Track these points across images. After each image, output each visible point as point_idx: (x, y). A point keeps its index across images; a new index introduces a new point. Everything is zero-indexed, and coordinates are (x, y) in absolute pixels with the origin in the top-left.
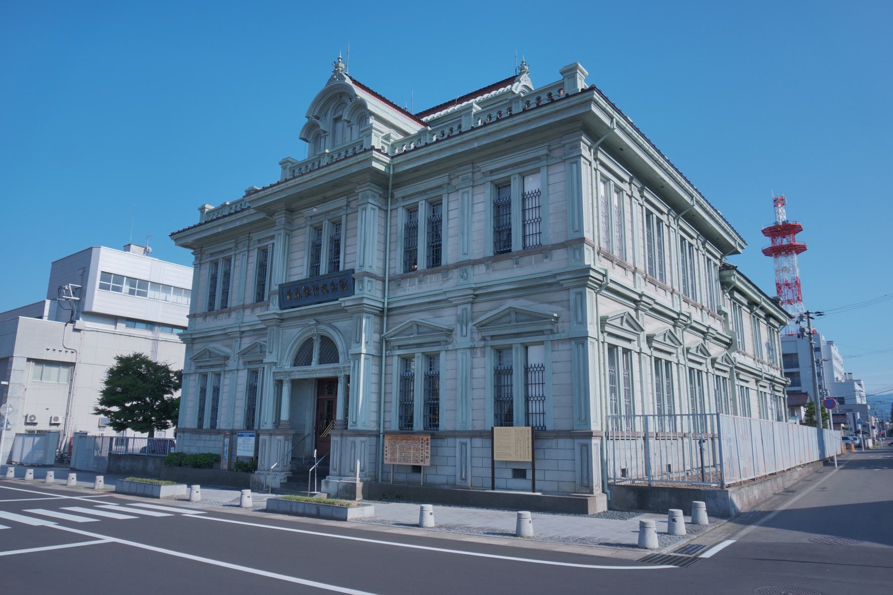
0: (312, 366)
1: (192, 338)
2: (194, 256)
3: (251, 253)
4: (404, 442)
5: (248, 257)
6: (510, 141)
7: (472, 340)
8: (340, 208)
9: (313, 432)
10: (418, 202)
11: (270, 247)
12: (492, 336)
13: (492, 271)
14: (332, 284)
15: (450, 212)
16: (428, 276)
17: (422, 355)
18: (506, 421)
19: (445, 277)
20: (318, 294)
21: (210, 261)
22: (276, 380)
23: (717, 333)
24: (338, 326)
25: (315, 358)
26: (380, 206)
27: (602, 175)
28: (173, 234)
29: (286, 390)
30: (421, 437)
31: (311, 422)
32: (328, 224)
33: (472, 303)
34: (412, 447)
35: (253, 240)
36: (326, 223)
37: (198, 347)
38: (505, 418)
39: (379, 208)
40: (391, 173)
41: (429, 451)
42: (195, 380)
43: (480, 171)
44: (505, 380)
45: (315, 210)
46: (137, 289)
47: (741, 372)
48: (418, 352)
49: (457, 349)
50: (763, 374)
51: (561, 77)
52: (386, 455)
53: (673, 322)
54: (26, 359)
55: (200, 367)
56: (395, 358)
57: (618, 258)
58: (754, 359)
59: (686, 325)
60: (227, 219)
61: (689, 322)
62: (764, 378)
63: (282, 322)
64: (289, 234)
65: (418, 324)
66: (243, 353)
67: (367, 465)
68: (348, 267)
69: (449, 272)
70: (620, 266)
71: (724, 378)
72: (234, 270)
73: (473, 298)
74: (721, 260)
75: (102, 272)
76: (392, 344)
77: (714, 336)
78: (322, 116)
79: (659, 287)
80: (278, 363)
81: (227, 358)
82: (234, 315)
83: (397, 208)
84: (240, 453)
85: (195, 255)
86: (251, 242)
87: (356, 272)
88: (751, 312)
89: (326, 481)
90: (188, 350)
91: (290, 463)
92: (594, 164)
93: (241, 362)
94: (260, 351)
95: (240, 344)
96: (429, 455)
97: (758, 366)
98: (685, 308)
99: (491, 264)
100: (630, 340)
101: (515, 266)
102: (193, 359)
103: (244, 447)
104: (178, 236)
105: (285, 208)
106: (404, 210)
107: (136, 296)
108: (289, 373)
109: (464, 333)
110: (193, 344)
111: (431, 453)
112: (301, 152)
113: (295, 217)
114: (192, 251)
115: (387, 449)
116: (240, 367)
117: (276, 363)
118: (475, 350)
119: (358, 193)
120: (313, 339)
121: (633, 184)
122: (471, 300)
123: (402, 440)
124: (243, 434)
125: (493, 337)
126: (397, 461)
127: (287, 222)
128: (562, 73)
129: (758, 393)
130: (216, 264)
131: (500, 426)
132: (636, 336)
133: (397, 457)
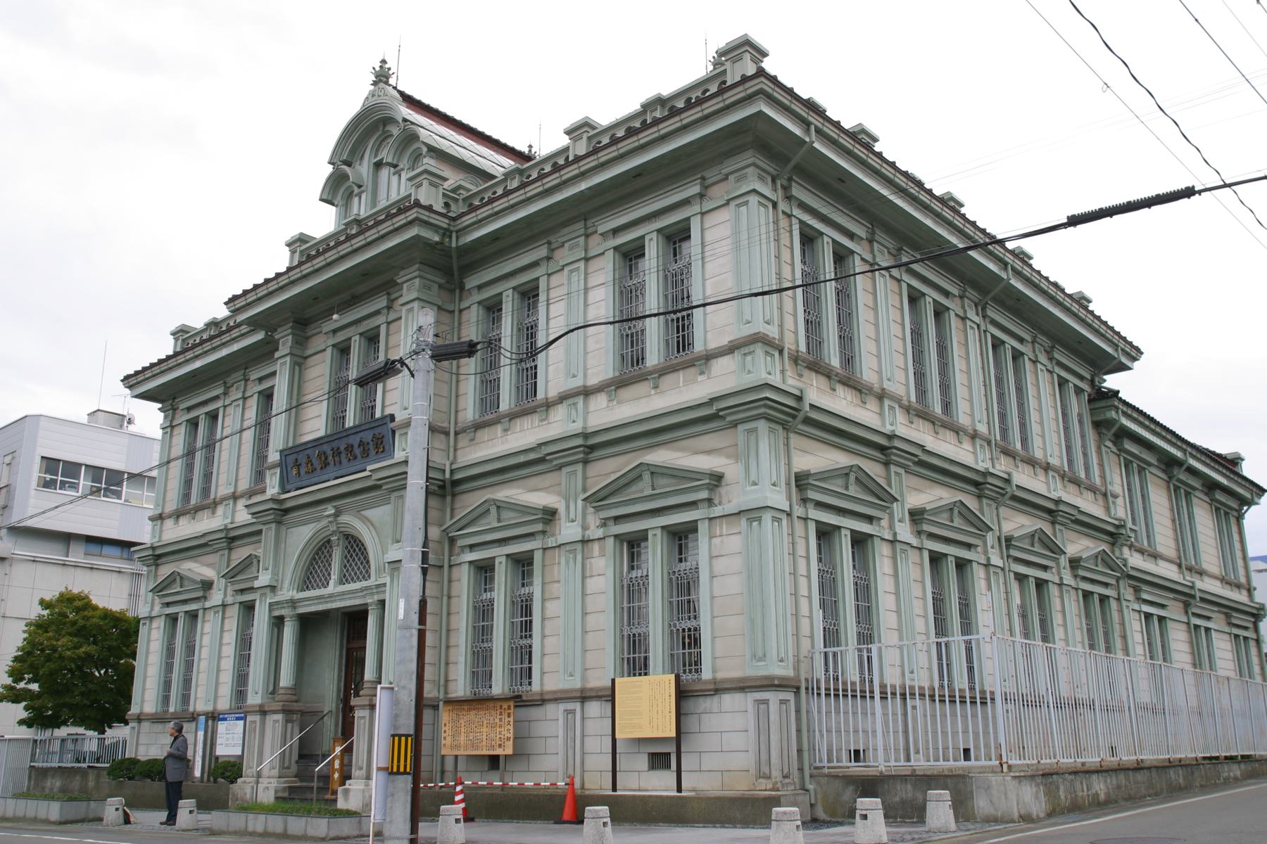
1: (156, 555)
2: (163, 414)
4: (473, 713)
6: (639, 175)
7: (585, 528)
9: (337, 708)
13: (619, 403)
14: (361, 444)
17: (507, 560)
19: (544, 420)
20: (340, 463)
21: (187, 421)
23: (1080, 512)
24: (374, 520)
25: (334, 574)
26: (440, 304)
28: (127, 378)
29: (289, 632)
31: (335, 689)
32: (360, 342)
33: (586, 462)
34: (485, 723)
36: (355, 341)
38: (637, 665)
41: (511, 728)
43: (596, 232)
46: (60, 478)
47: (1144, 587)
48: (499, 553)
50: (1197, 592)
52: (445, 738)
53: (977, 491)
55: (168, 604)
56: (465, 567)
57: (839, 371)
58: (1180, 566)
60: (207, 346)
62: (1198, 599)
63: (284, 515)
64: (300, 362)
65: (498, 504)
68: (388, 411)
69: (549, 411)
70: (849, 386)
71: (1246, 638)
73: (584, 452)
74: (1092, 382)
75: (42, 457)
76: (460, 543)
77: (1074, 518)
78: (356, 161)
79: (941, 426)
80: (279, 587)
81: (207, 585)
82: (220, 510)
84: (220, 751)
85: (164, 412)
88: (1170, 478)
91: (297, 762)
92: (782, 206)
93: (229, 592)
96: (511, 735)
97: (1188, 578)
98: (1002, 466)
99: (615, 390)
100: (1045, 568)
102: (156, 590)
104: (133, 381)
105: (292, 320)
107: (103, 499)
108: (293, 603)
109: (572, 516)
110: (157, 565)
111: (514, 734)
113: (309, 334)
115: (446, 729)
117: (274, 587)
121: (878, 242)
122: (581, 456)
124: (226, 716)
125: (617, 519)
126: (462, 750)
127: (297, 343)
128: (568, 132)
129: (1189, 627)
132: (980, 539)
133: (462, 743)
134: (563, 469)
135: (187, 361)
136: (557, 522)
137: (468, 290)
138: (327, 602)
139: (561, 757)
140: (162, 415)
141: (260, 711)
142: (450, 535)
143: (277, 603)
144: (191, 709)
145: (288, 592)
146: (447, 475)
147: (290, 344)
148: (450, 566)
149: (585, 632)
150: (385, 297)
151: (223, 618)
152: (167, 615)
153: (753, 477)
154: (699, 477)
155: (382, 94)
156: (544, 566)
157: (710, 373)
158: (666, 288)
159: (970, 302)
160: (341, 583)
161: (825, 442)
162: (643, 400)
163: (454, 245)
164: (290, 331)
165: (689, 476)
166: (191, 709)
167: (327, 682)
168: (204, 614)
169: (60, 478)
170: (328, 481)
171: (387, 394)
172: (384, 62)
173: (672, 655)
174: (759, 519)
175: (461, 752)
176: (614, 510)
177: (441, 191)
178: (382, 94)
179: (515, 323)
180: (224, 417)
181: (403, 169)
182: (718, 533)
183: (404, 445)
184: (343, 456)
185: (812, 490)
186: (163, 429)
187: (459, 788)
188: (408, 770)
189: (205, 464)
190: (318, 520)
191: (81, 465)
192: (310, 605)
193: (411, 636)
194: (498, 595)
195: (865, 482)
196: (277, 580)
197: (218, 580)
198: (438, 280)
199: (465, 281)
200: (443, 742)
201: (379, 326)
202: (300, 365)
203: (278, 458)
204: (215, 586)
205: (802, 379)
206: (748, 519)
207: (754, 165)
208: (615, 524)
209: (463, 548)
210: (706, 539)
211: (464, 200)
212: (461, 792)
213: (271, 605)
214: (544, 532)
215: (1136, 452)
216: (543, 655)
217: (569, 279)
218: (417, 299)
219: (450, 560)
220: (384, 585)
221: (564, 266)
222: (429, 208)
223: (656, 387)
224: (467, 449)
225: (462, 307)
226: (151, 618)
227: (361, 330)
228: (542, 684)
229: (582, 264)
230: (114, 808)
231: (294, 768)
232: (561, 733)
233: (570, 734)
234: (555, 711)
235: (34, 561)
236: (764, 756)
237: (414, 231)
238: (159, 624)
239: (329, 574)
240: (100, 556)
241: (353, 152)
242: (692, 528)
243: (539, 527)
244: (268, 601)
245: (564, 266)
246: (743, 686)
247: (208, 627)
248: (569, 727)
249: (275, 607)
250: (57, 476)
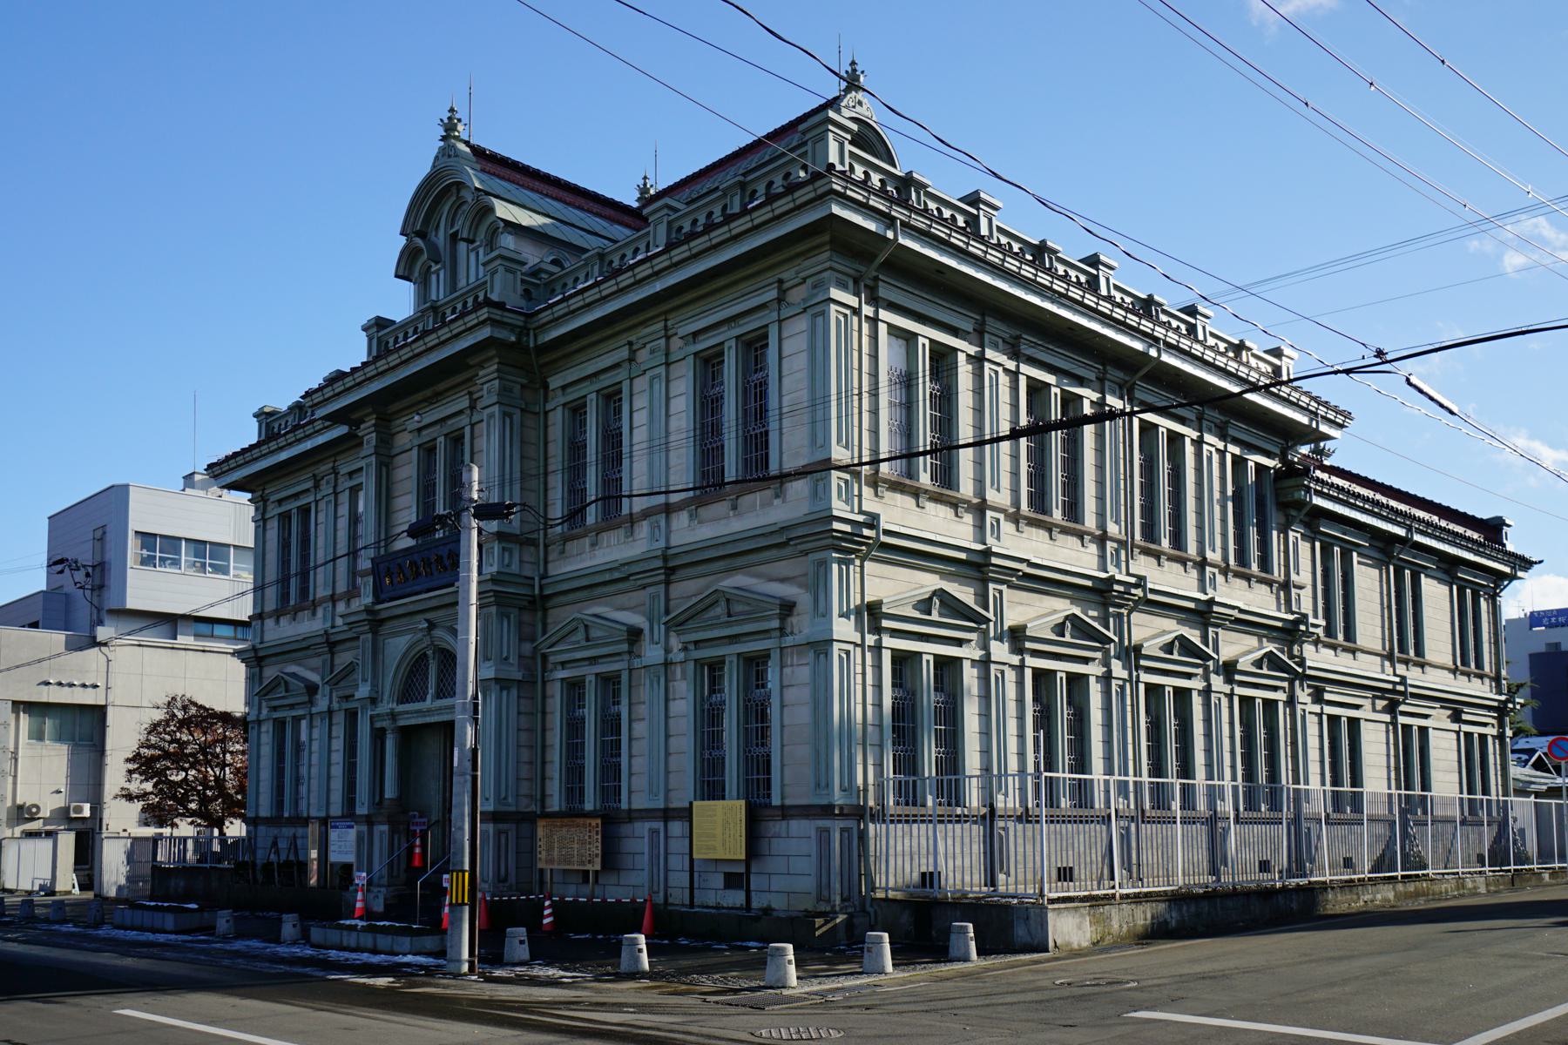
3: (676, 370)
5: (668, 381)
7: (667, 650)
8: (460, 412)
11: (591, 400)
12: (696, 643)
13: (699, 523)
16: (605, 535)
20: (432, 574)
26: (523, 406)
27: (894, 330)
28: (210, 466)
30: (588, 821)
37: (270, 673)
38: (712, 789)
40: (532, 345)
41: (599, 845)
48: (589, 672)
52: (540, 853)
54: (10, 703)
55: (275, 709)
56: (558, 685)
63: (380, 626)
72: (316, 529)
73: (665, 573)
75: (136, 532)
82: (643, 529)
84: (334, 857)
86: (268, 503)
90: (251, 679)
93: (675, 643)
94: (584, 636)
96: (599, 852)
101: (731, 513)
103: (340, 847)
104: (217, 470)
108: (393, 716)
112: (400, 302)
113: (394, 431)
114: (249, 496)
118: (673, 667)
119: (482, 384)
123: (562, 826)
131: (709, 799)
135: (272, 452)
137: (553, 390)
138: (425, 716)
139: (645, 875)
143: (378, 715)
145: (385, 707)
146: (537, 592)
147: (374, 442)
149: (667, 754)
151: (330, 725)
156: (630, 687)
157: (785, 496)
158: (745, 403)
159: (1114, 385)
162: (723, 522)
163: (532, 345)
169: (158, 554)
172: (452, 110)
173: (747, 780)
175: (555, 867)
176: (694, 634)
177: (519, 276)
179: (600, 431)
180: (316, 513)
182: (789, 663)
183: (491, 561)
184: (434, 567)
186: (255, 522)
187: (547, 903)
188: (466, 901)
189: (301, 562)
191: (180, 539)
193: (465, 781)
194: (589, 714)
195: (952, 606)
196: (377, 692)
197: (323, 685)
199: (549, 380)
200: (539, 856)
201: (463, 428)
202: (387, 466)
203: (370, 566)
204: (320, 691)
205: (884, 501)
206: (815, 652)
207: (831, 268)
208: (696, 649)
209: (555, 664)
211: (545, 284)
212: (549, 907)
213: (372, 717)
216: (630, 775)
217: (651, 386)
221: (645, 371)
222: (500, 306)
223: (734, 508)
224: (557, 563)
225: (548, 408)
228: (630, 803)
230: (225, 920)
232: (646, 850)
233: (655, 852)
234: (643, 828)
235: (139, 645)
236: (824, 880)
238: (267, 728)
239: (427, 688)
240: (212, 636)
242: (765, 656)
244: (369, 713)
245: (645, 371)
246: (807, 812)
247: (641, 402)
248: (653, 845)
250: (155, 552)
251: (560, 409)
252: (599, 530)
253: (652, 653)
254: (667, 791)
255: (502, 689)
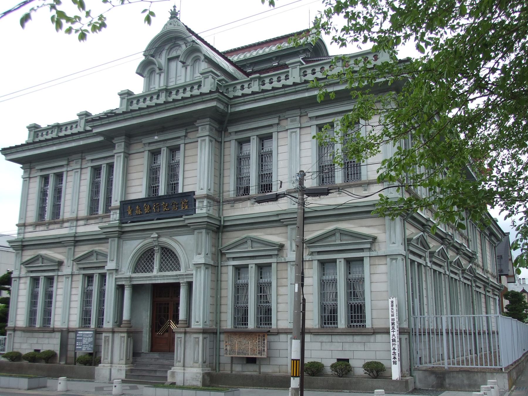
0: (153, 273)
10: (250, 137)
15: (279, 147)
18: (352, 322)
22: (118, 285)
35: (87, 159)
39: (216, 140)
42: (25, 283)
44: (329, 290)
45: (156, 137)
49: (287, 262)
51: (77, 118)
55: (32, 272)
59: (450, 243)
61: (452, 242)
63: (122, 234)
64: (127, 156)
65: (252, 239)
66: (78, 260)
67: (208, 357)
68: (187, 189)
73: (22, 247)
77: (464, 252)
81: (60, 263)
83: (230, 141)
87: (196, 193)
89: (172, 372)
95: (74, 252)
106: (236, 143)
114: (21, 166)
116: (76, 272)
120: (154, 250)
125: (319, 253)
128: (79, 115)
130: (46, 179)
134: (288, 226)
136: (284, 251)
140: (23, 170)
141: (112, 331)
142: (223, 252)
144: (52, 326)
148: (221, 266)
150: (185, 131)
152: (31, 277)
153: (393, 241)
154: (367, 238)
155: (176, 24)
160: (160, 271)
161: (414, 226)
164: (123, 140)
165: (358, 236)
166: (52, 326)
167: (144, 317)
168: (58, 279)
170: (153, 220)
171: (185, 179)
172: (175, 7)
174: (396, 259)
178: (176, 24)
181: (188, 65)
185: (411, 246)
190: (145, 238)
192: (146, 280)
198: (215, 126)
199: (228, 128)
209: (228, 259)
210: (368, 266)
211: (225, 86)
213: (116, 278)
214: (277, 255)
215: (107, 122)
218: (209, 136)
219: (221, 263)
220: (192, 274)
226: (20, 278)
227: (168, 145)
229: (79, 170)
231: (131, 360)
237: (213, 104)
241: (155, 52)
243: (276, 252)
249: (118, 280)
251: (89, 169)
252: (50, 223)
253: (66, 270)
254: (69, 321)
255: (206, 268)
